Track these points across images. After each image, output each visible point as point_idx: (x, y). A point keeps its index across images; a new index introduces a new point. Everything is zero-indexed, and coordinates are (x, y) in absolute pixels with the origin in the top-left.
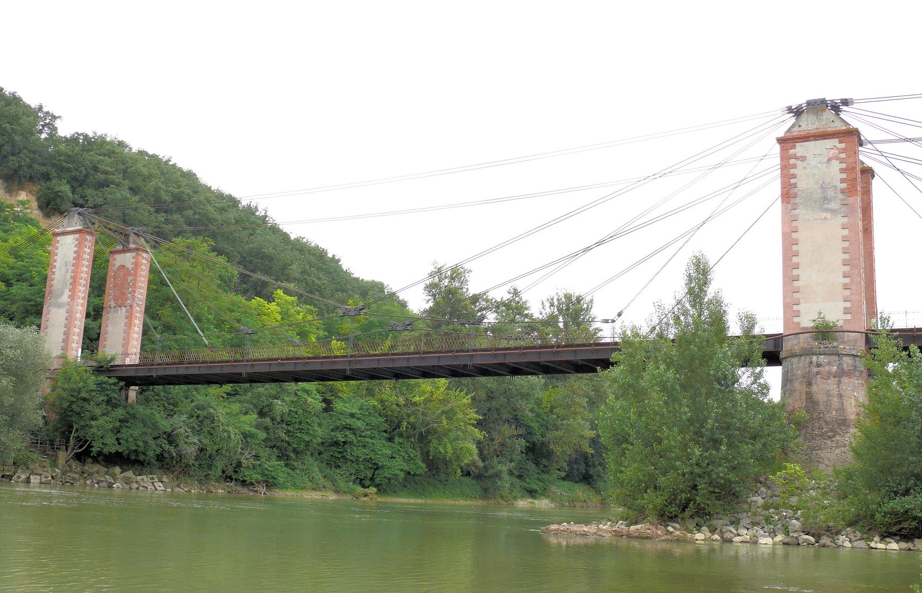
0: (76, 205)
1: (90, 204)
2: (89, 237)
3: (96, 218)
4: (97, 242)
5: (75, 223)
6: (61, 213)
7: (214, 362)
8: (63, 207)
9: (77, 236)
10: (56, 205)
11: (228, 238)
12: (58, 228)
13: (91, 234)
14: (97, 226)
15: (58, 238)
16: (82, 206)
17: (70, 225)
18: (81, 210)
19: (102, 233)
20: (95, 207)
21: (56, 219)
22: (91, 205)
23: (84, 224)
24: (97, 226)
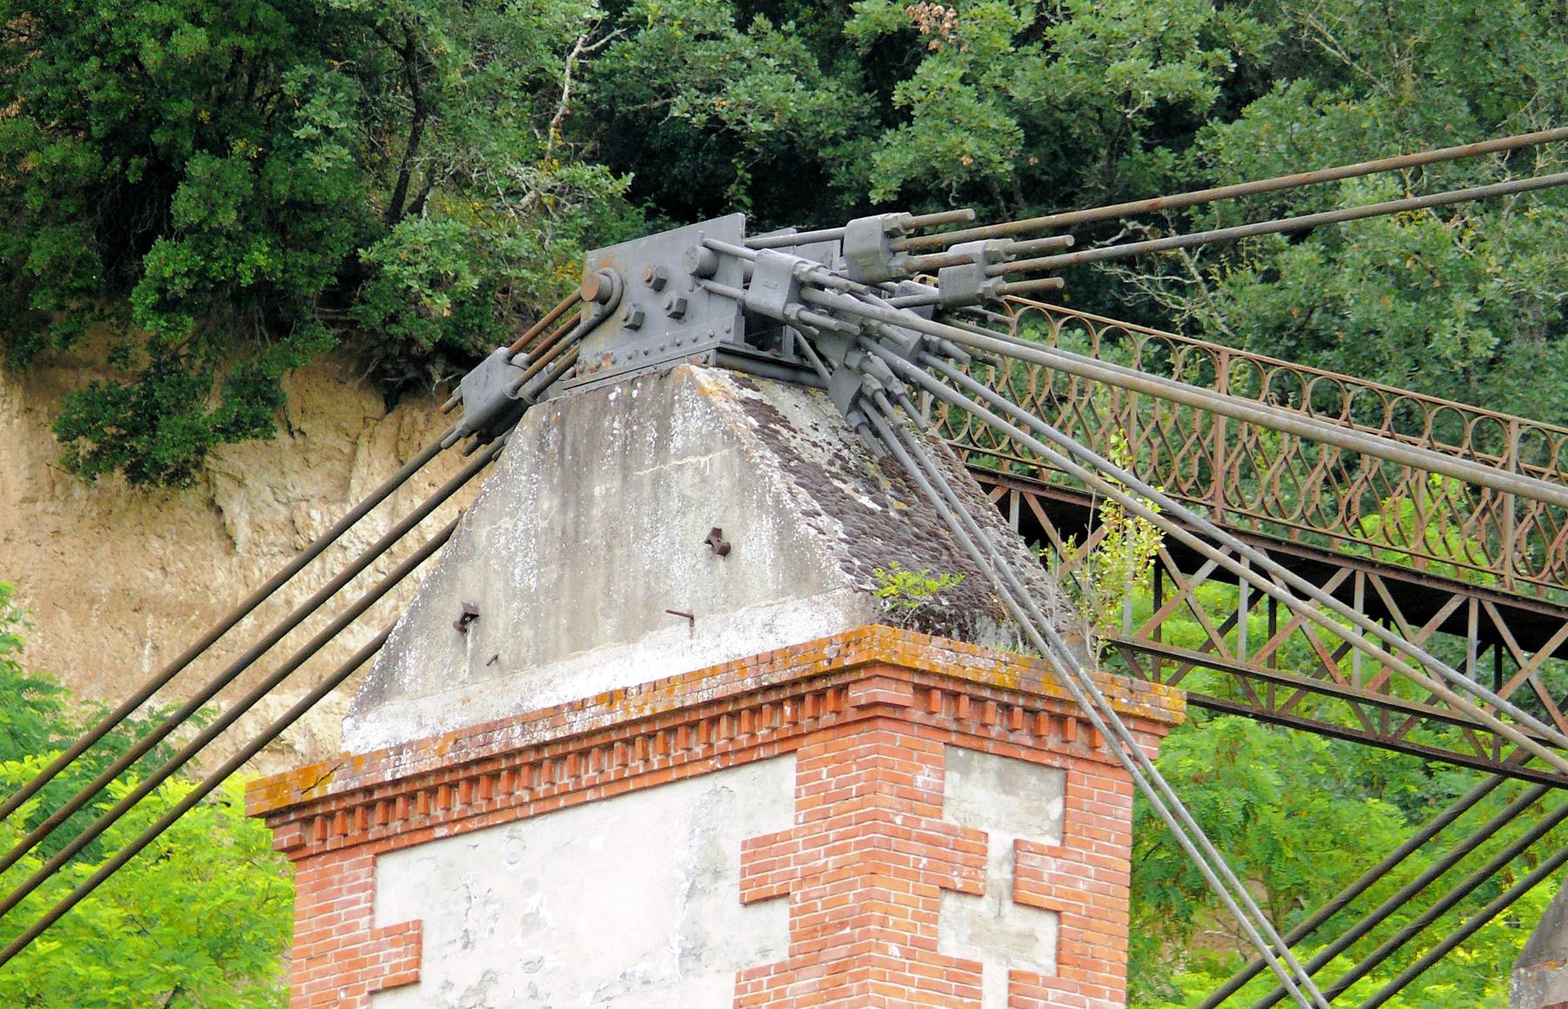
0: (670, 168)
1: (957, 118)
2: (994, 804)
3: (1103, 404)
4: (1164, 885)
5: (669, 522)
6: (406, 372)
7: (868, 719)
8: (428, 248)
9: (764, 797)
10: (287, 219)
11: (366, 114)
12: (372, 676)
13: (1032, 722)
14: (1127, 550)
15: (405, 884)
16: (795, 188)
17: (586, 583)
18: (779, 264)
19: (1246, 696)
20: (1057, 163)
21: (304, 494)
22: (980, 139)
23: (871, 542)
24: (1127, 550)
